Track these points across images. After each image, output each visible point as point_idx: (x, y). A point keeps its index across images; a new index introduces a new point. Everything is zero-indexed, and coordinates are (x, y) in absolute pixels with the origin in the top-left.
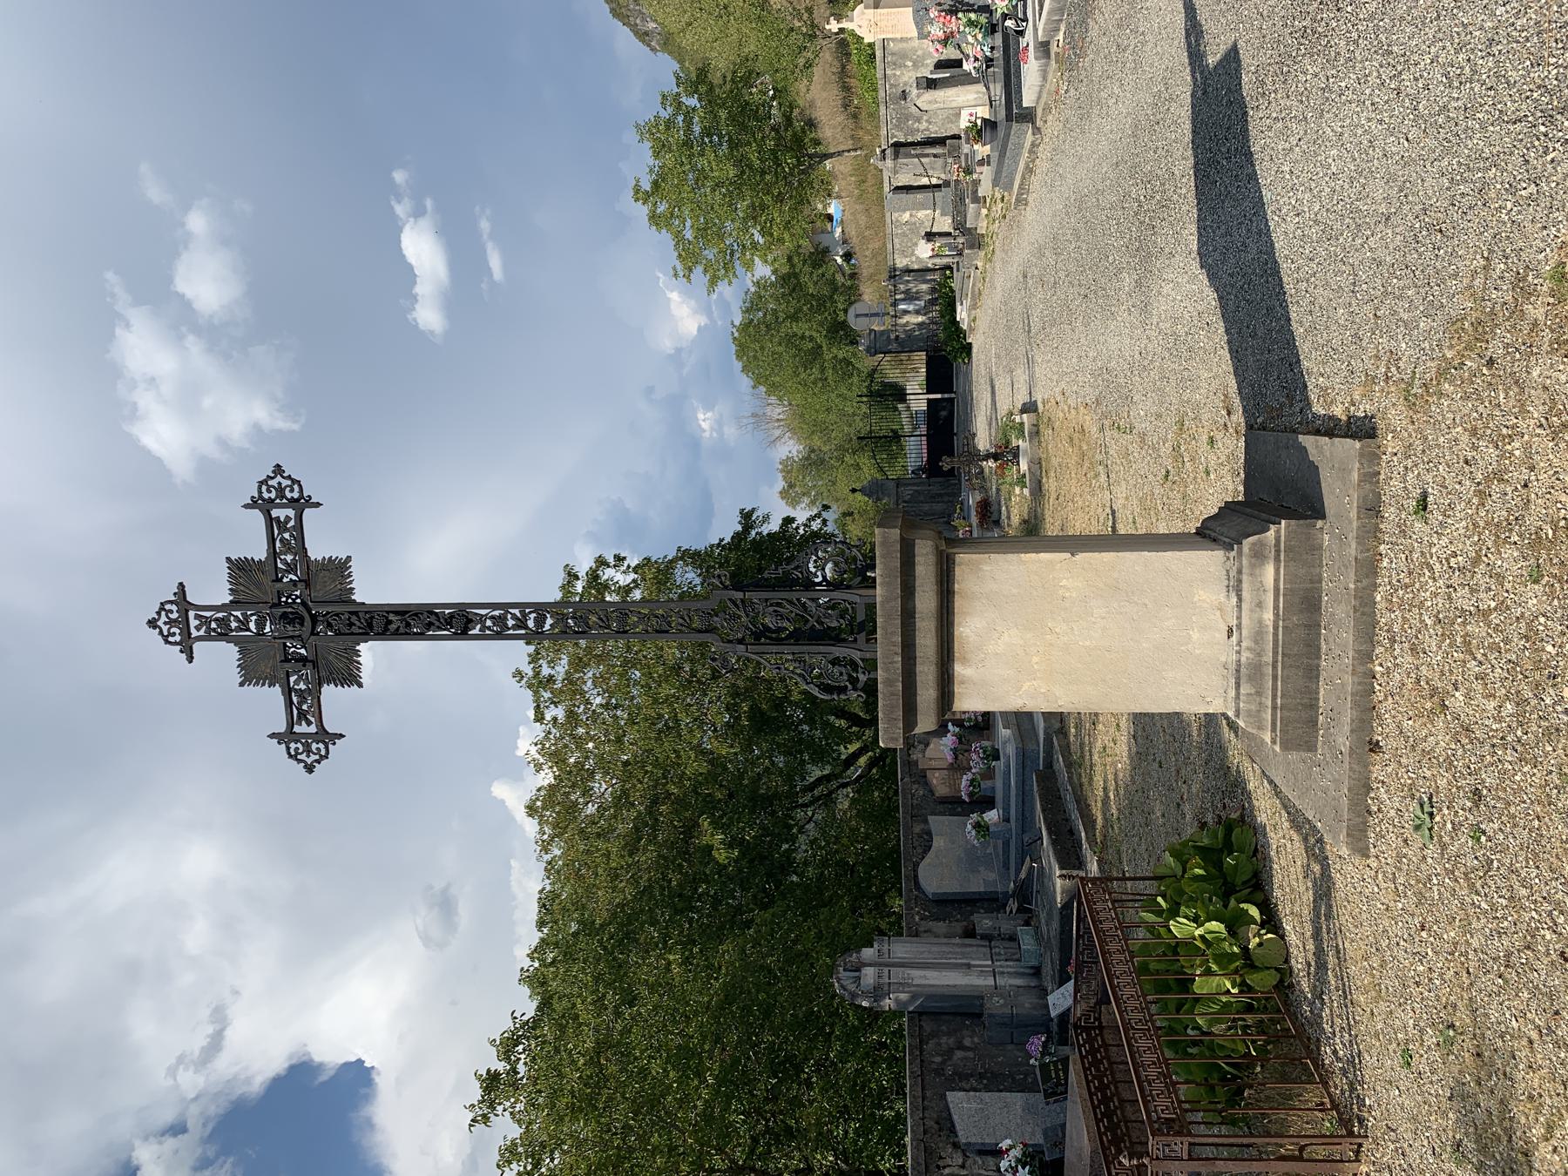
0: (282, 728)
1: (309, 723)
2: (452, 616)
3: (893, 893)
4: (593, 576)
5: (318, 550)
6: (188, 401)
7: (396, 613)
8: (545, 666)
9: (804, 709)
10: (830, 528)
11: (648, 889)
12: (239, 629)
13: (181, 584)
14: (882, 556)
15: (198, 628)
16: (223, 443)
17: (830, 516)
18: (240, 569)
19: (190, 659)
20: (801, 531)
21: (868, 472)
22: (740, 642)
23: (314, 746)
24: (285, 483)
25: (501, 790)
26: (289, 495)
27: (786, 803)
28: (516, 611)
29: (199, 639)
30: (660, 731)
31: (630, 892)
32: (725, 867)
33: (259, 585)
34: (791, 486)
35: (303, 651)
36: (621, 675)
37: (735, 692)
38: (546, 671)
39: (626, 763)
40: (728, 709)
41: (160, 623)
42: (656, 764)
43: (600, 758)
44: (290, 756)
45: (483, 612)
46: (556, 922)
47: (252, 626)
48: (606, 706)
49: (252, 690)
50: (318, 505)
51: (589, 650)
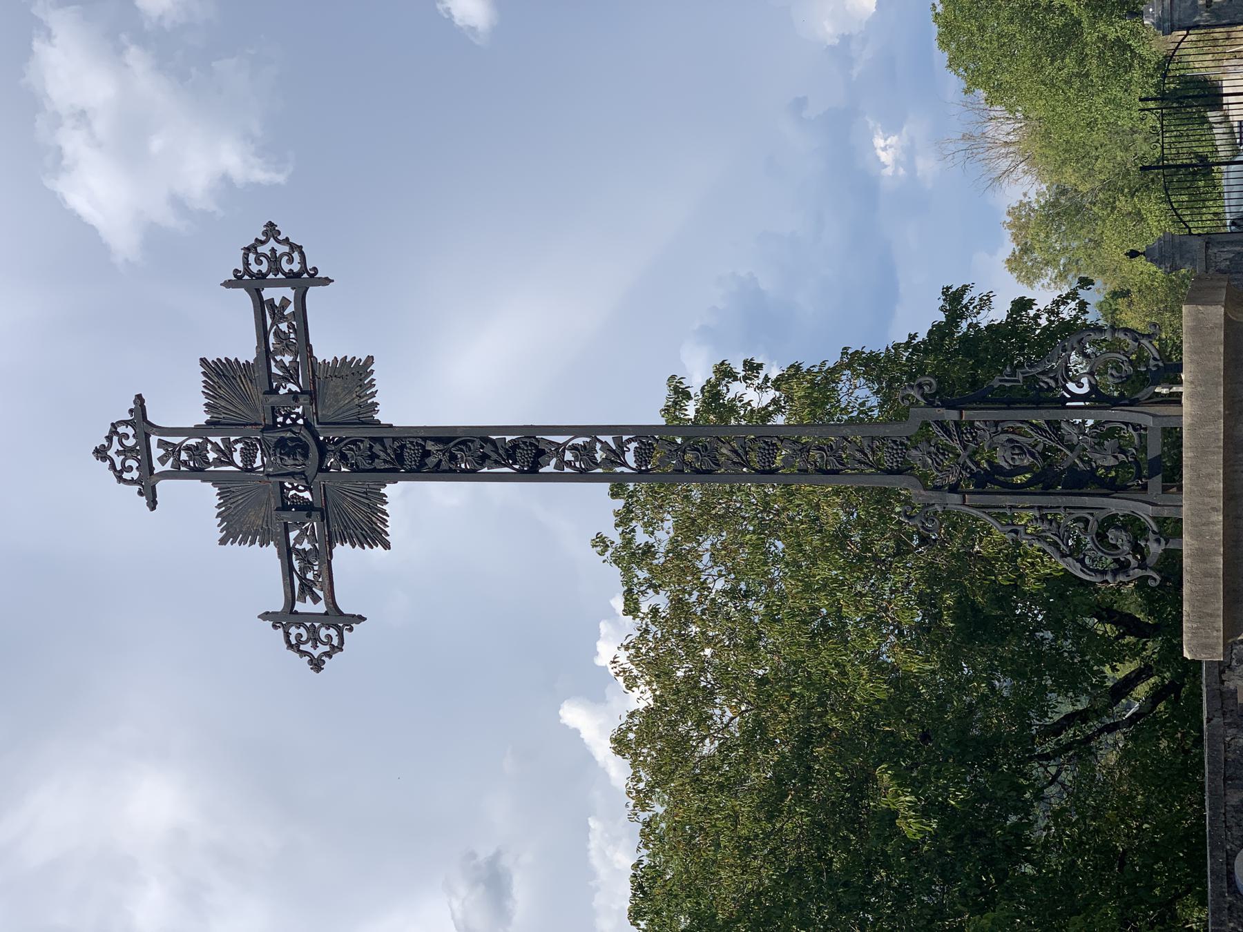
0: (278, 605)
1: (316, 599)
2: (515, 445)
3: (1190, 899)
4: (712, 394)
5: (327, 347)
6: (130, 141)
7: (437, 440)
8: (640, 530)
9: (1045, 605)
10: (1092, 316)
11: (795, 874)
12: (218, 462)
13: (139, 397)
14: (1194, 351)
15: (162, 460)
16: (178, 203)
17: (1092, 296)
18: (220, 376)
19: (153, 504)
20: (1043, 322)
21: (1157, 223)
22: (954, 489)
23: (323, 633)
24: (282, 249)
25: (574, 715)
26: (286, 267)
27: (1016, 752)
28: (609, 439)
29: (165, 475)
30: (813, 636)
31: (769, 874)
32: (916, 845)
33: (245, 398)
34: (1026, 250)
35: (307, 495)
36: (756, 547)
37: (932, 576)
38: (641, 538)
39: (762, 681)
40: (921, 602)
41: (111, 453)
42: (809, 683)
43: (723, 671)
44: (290, 646)
45: (560, 439)
46: (658, 913)
47: (237, 457)
48: (732, 593)
49: (235, 550)
50: (327, 281)
51: (706, 506)
